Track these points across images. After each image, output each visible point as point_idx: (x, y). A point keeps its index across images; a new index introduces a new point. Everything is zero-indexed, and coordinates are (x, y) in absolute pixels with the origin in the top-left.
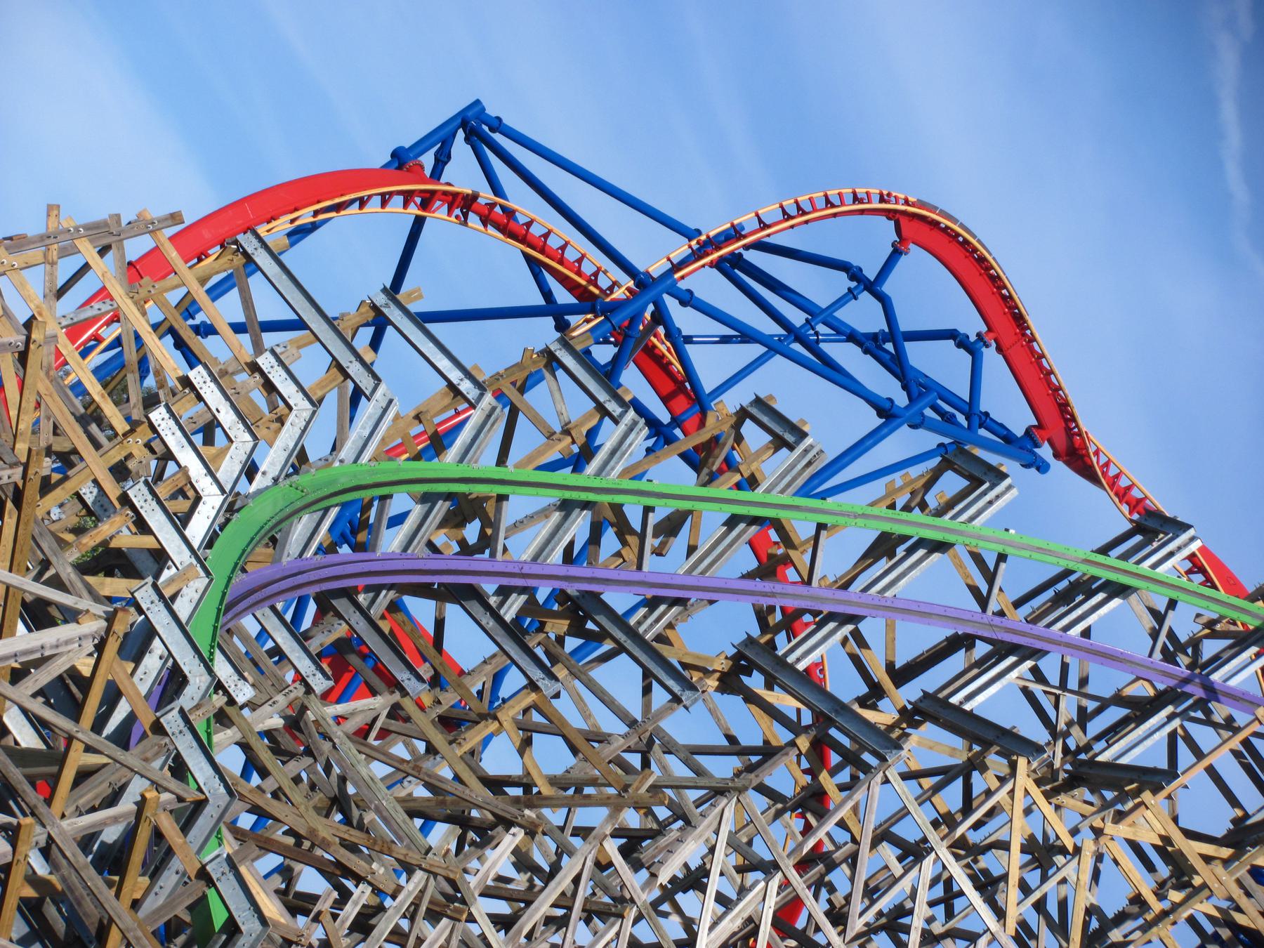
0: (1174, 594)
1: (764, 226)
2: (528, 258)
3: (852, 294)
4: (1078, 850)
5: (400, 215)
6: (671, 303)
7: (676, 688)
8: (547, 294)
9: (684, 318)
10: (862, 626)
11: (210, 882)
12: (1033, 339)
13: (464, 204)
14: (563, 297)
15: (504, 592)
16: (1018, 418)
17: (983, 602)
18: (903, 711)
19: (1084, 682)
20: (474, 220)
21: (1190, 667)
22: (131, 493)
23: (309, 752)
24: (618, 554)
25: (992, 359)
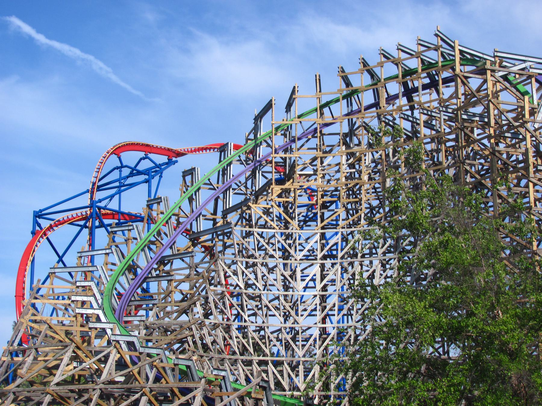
0: (238, 155)
1: (97, 178)
2: (69, 224)
3: (120, 171)
4: (272, 206)
5: (44, 241)
6: (99, 204)
7: (190, 255)
8: (78, 225)
9: (102, 204)
10: (203, 214)
11: (177, 365)
12: (153, 146)
13: (51, 228)
14: (82, 223)
15: (150, 272)
16: (164, 159)
17: (214, 189)
18: (222, 218)
19: (240, 182)
20: (55, 228)
21: (252, 162)
22: (90, 326)
23: (154, 330)
24: (157, 247)
25: (151, 156)
